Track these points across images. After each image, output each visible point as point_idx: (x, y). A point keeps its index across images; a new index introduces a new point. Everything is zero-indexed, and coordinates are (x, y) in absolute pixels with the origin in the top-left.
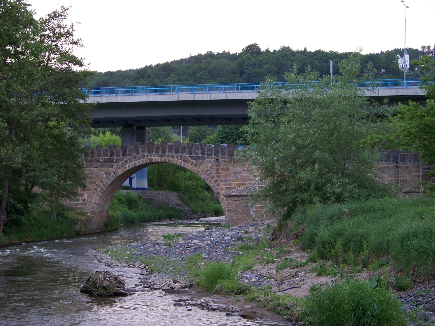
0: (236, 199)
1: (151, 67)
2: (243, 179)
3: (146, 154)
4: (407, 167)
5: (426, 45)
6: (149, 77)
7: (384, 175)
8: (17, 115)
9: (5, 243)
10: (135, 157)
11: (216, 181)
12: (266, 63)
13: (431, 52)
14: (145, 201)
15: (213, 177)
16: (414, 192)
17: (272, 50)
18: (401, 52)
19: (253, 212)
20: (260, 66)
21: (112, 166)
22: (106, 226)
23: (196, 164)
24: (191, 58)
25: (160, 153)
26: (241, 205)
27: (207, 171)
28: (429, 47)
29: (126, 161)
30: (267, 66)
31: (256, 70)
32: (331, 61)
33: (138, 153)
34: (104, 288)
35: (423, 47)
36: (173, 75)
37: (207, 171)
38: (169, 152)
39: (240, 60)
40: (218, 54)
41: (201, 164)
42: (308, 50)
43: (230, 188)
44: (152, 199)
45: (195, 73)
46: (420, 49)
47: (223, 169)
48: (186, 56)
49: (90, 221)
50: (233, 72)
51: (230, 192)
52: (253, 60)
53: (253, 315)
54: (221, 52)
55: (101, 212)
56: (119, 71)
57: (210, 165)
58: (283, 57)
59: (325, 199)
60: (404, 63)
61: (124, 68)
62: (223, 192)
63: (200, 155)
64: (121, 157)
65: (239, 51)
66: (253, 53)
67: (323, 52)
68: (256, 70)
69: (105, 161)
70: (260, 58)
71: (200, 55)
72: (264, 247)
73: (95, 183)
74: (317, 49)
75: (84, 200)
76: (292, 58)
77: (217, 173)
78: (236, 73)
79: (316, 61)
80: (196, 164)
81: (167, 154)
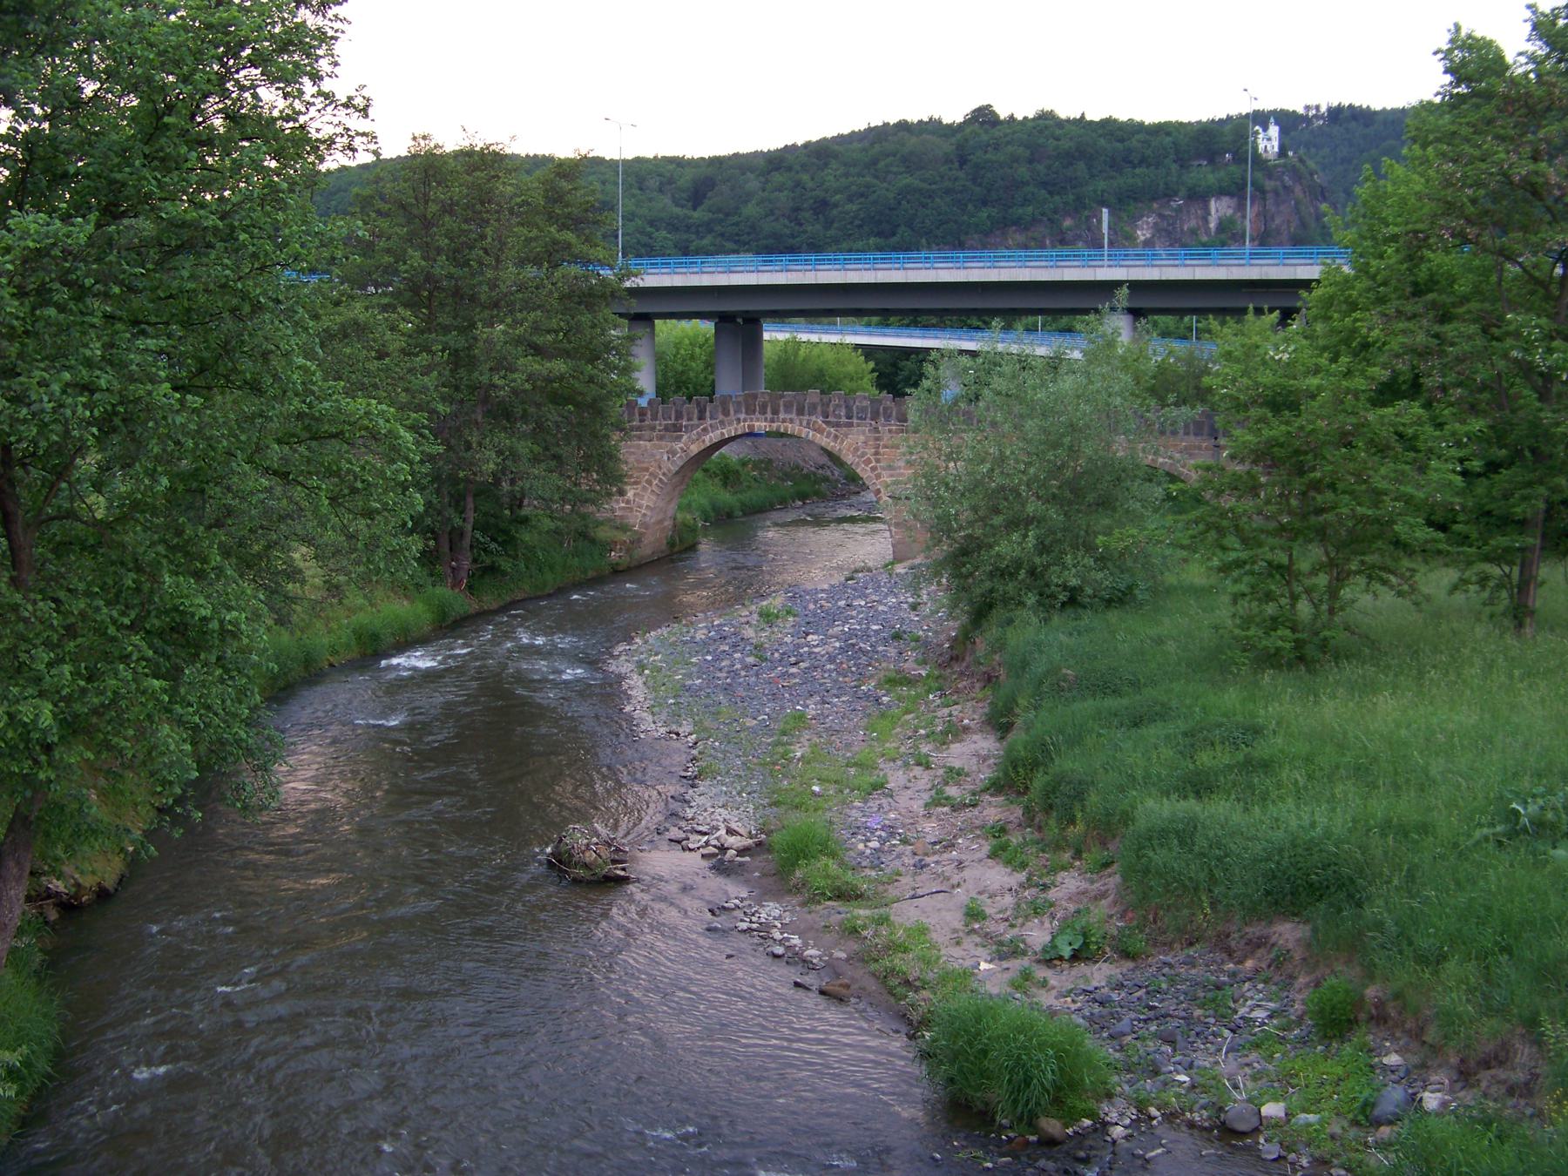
1: (794, 146)
3: (742, 416)
5: (1314, 103)
6: (790, 169)
8: (485, 379)
9: (471, 611)
10: (722, 423)
11: (873, 469)
12: (1008, 143)
13: (1322, 117)
14: (756, 465)
15: (868, 462)
17: (1019, 117)
18: (1261, 118)
20: (997, 147)
21: (679, 438)
22: (671, 544)
23: (836, 437)
24: (870, 130)
25: (769, 415)
27: (857, 449)
28: (1317, 108)
29: (705, 430)
30: (1010, 149)
31: (988, 156)
32: (1105, 210)
33: (726, 414)
34: (586, 866)
35: (1307, 108)
36: (834, 164)
37: (857, 449)
38: (786, 412)
39: (959, 136)
40: (920, 122)
41: (846, 436)
42: (1088, 118)
44: (770, 461)
45: (875, 162)
46: (1301, 111)
47: (885, 447)
48: (861, 126)
49: (639, 540)
50: (948, 161)
52: (985, 138)
53: (844, 991)
54: (926, 119)
55: (661, 522)
56: (736, 155)
57: (862, 438)
58: (1041, 132)
59: (1047, 602)
60: (1268, 142)
61: (746, 146)
63: (844, 420)
64: (695, 421)
65: (960, 119)
66: (984, 122)
67: (1115, 121)
68: (988, 156)
69: (666, 429)
70: (996, 132)
71: (886, 125)
72: (928, 692)
73: (647, 469)
74: (1105, 116)
75: (628, 502)
76: (1058, 132)
77: (876, 453)
78: (952, 162)
79: (1102, 141)
80: (836, 437)
81: (782, 416)
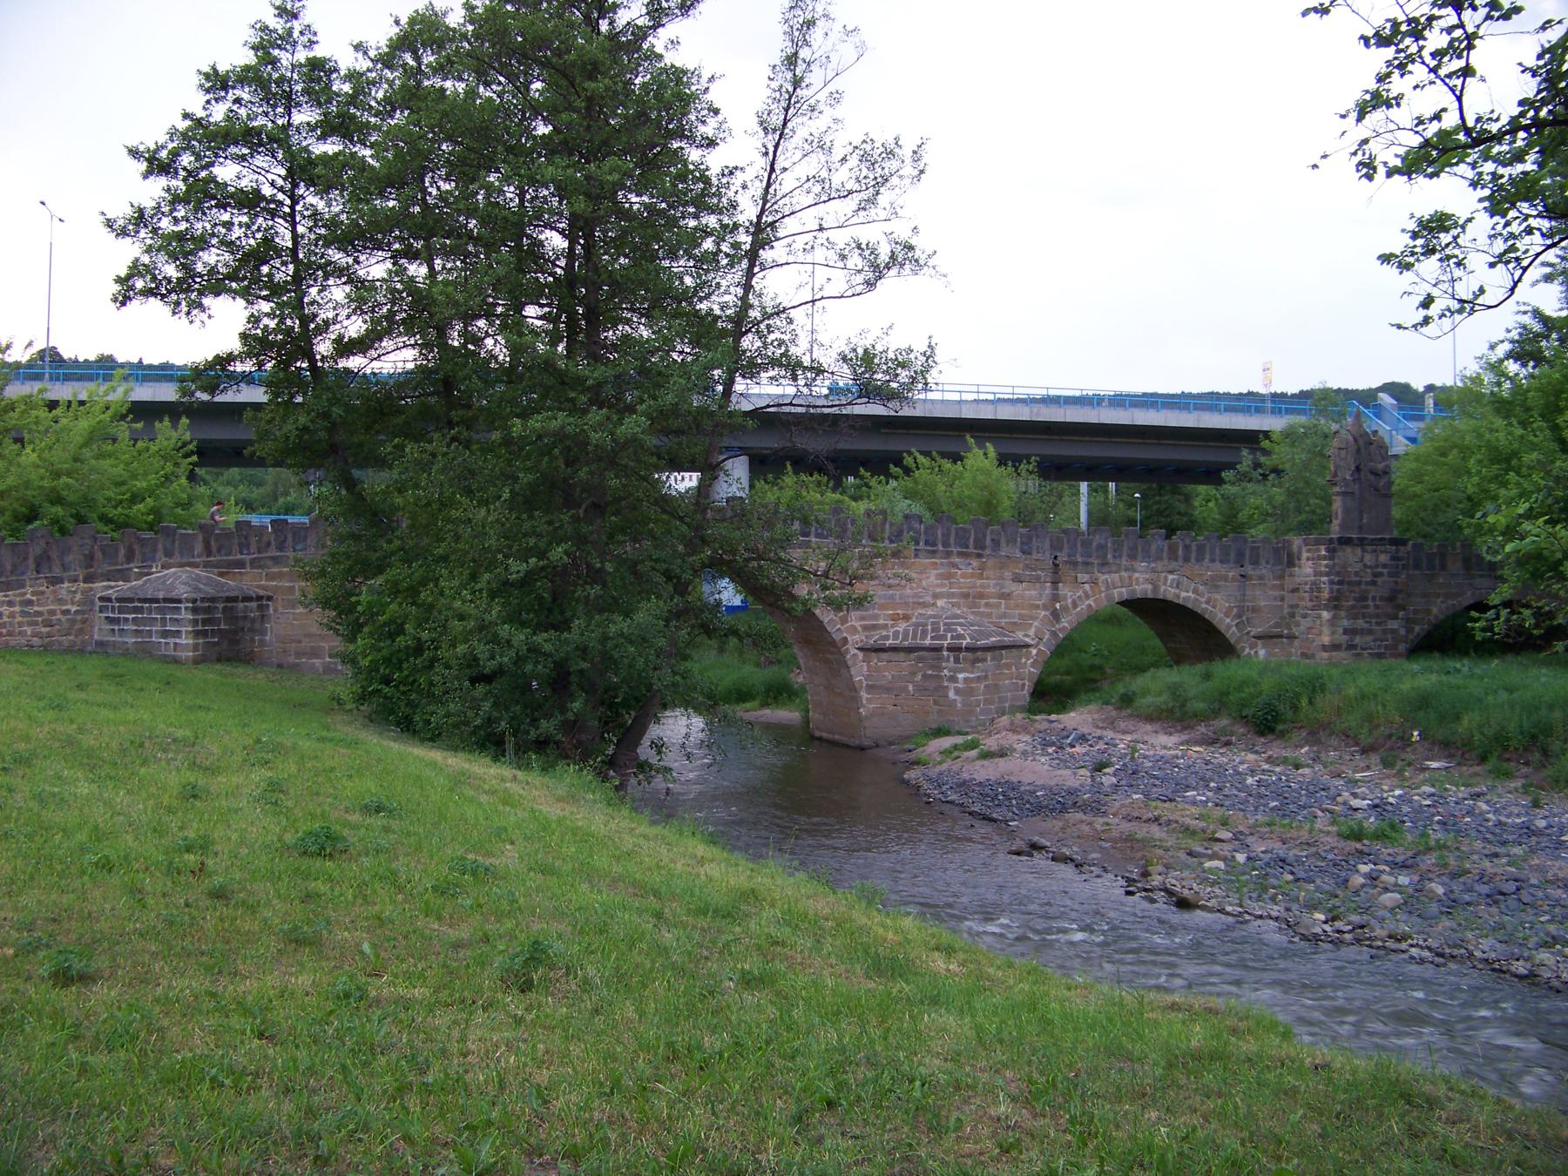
0: (902, 656)
2: (907, 603)
4: (1261, 578)
7: (1217, 596)
16: (1281, 636)
19: (957, 691)
26: (914, 674)
43: (874, 627)
51: (874, 639)
62: (856, 639)
